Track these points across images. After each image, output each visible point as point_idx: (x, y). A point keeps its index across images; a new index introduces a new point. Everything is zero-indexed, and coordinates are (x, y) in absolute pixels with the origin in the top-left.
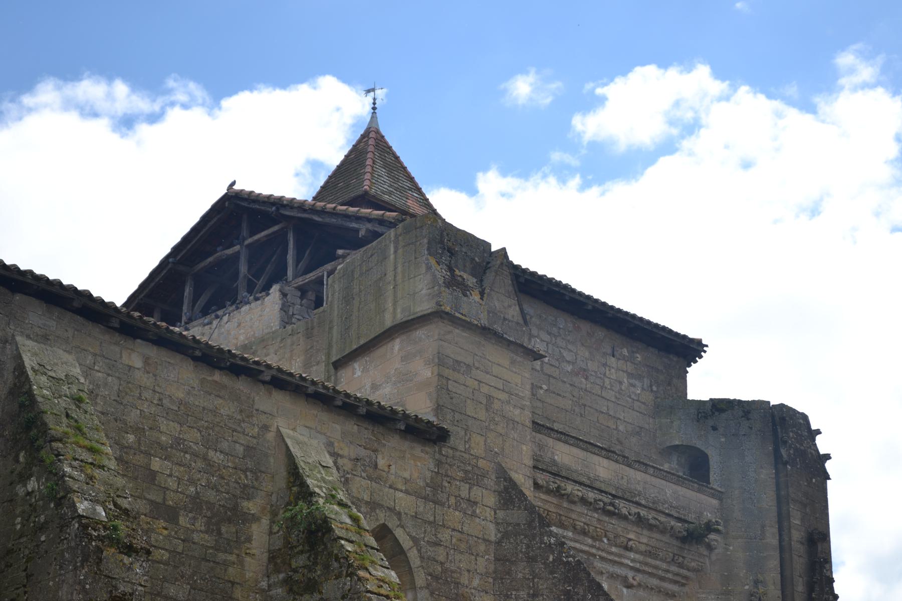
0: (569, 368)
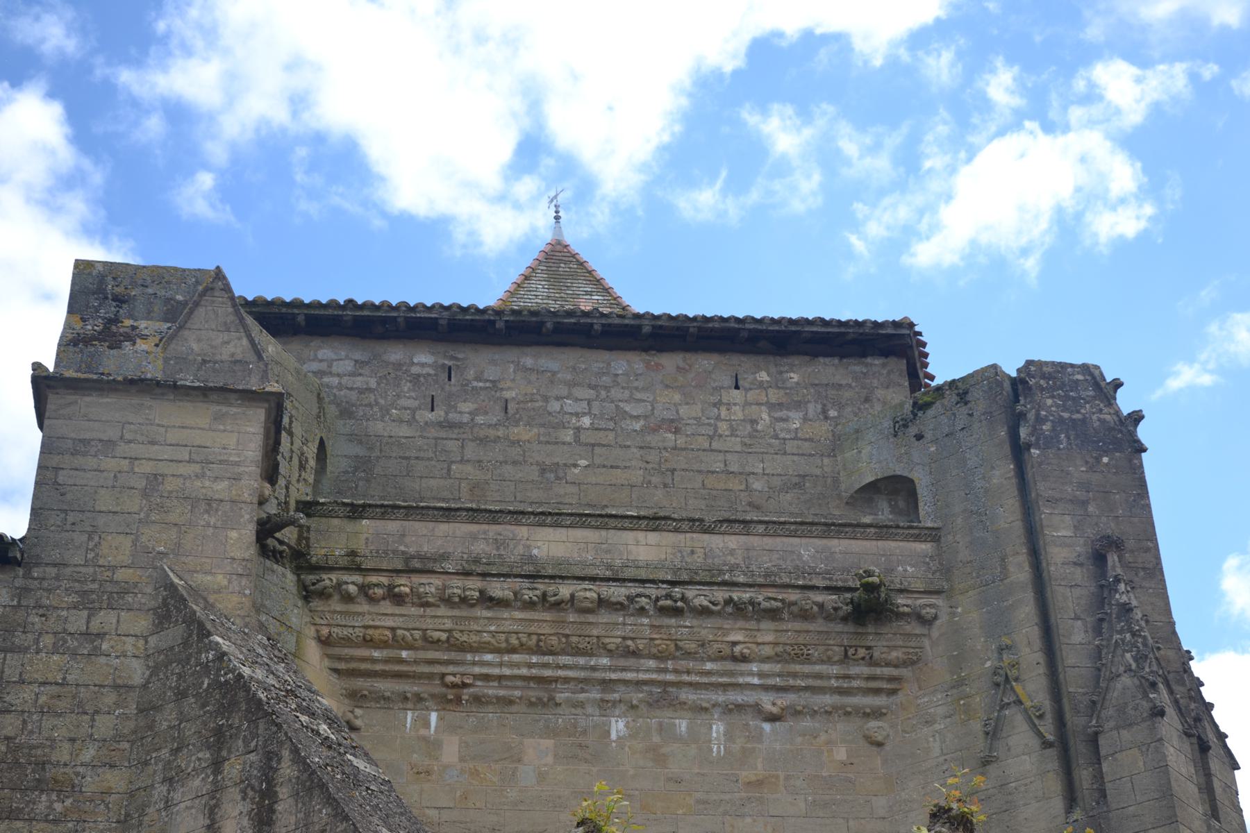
0: (638, 426)
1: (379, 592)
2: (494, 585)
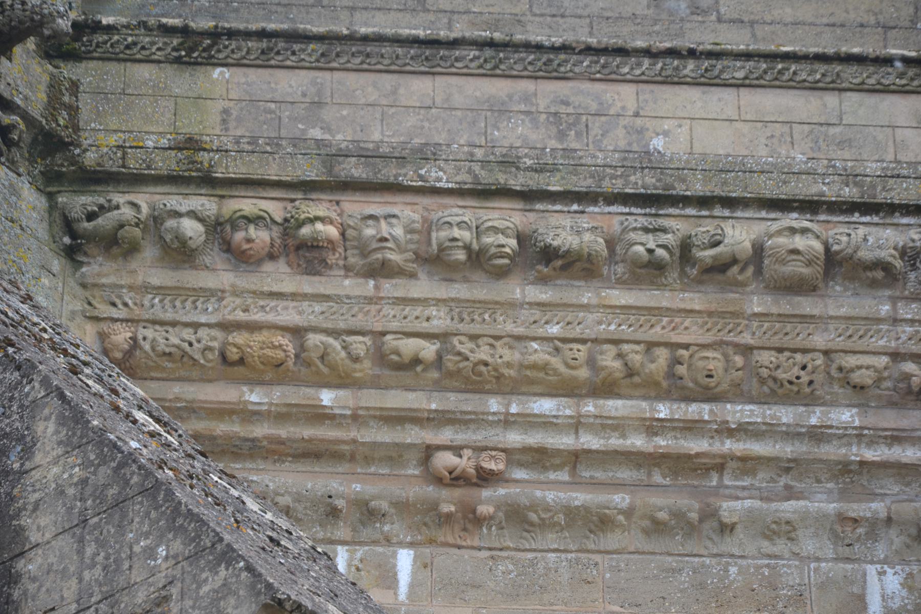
1: (261, 236)
2: (554, 220)
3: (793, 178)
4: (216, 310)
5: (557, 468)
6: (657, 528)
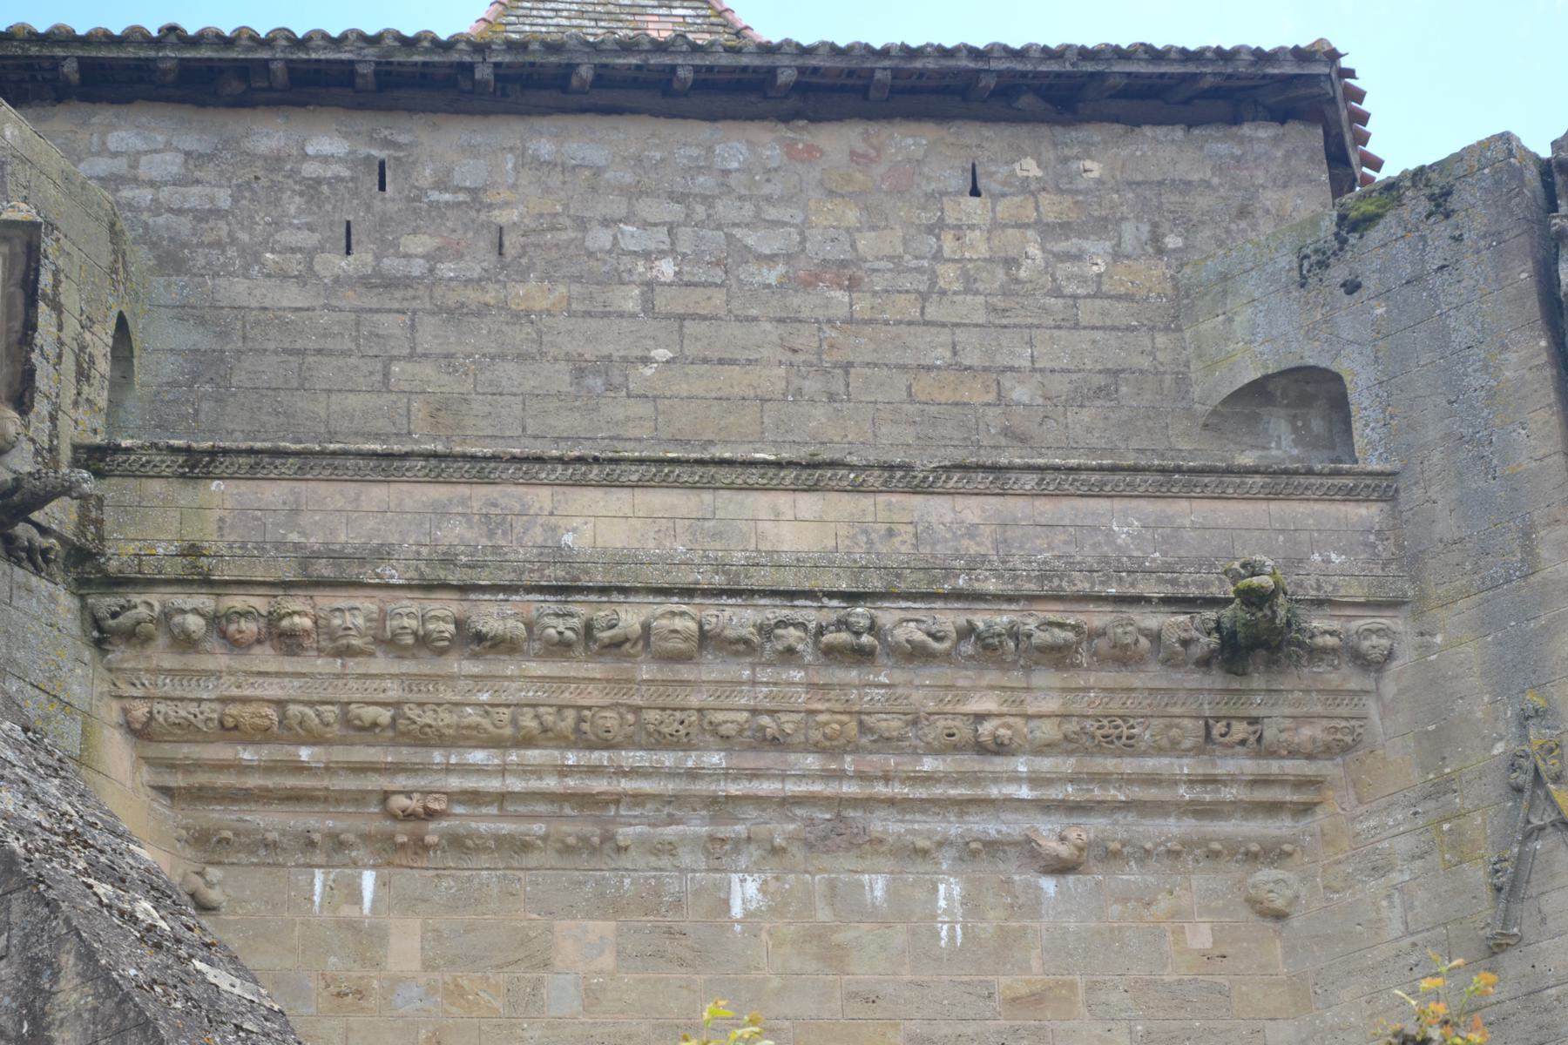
1: (250, 627)
3: (675, 568)
4: (216, 687)
5: (487, 804)
6: (567, 850)
